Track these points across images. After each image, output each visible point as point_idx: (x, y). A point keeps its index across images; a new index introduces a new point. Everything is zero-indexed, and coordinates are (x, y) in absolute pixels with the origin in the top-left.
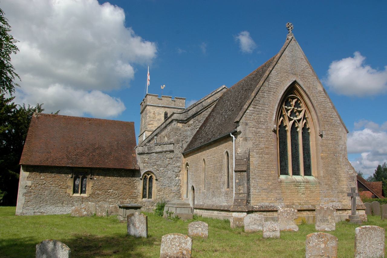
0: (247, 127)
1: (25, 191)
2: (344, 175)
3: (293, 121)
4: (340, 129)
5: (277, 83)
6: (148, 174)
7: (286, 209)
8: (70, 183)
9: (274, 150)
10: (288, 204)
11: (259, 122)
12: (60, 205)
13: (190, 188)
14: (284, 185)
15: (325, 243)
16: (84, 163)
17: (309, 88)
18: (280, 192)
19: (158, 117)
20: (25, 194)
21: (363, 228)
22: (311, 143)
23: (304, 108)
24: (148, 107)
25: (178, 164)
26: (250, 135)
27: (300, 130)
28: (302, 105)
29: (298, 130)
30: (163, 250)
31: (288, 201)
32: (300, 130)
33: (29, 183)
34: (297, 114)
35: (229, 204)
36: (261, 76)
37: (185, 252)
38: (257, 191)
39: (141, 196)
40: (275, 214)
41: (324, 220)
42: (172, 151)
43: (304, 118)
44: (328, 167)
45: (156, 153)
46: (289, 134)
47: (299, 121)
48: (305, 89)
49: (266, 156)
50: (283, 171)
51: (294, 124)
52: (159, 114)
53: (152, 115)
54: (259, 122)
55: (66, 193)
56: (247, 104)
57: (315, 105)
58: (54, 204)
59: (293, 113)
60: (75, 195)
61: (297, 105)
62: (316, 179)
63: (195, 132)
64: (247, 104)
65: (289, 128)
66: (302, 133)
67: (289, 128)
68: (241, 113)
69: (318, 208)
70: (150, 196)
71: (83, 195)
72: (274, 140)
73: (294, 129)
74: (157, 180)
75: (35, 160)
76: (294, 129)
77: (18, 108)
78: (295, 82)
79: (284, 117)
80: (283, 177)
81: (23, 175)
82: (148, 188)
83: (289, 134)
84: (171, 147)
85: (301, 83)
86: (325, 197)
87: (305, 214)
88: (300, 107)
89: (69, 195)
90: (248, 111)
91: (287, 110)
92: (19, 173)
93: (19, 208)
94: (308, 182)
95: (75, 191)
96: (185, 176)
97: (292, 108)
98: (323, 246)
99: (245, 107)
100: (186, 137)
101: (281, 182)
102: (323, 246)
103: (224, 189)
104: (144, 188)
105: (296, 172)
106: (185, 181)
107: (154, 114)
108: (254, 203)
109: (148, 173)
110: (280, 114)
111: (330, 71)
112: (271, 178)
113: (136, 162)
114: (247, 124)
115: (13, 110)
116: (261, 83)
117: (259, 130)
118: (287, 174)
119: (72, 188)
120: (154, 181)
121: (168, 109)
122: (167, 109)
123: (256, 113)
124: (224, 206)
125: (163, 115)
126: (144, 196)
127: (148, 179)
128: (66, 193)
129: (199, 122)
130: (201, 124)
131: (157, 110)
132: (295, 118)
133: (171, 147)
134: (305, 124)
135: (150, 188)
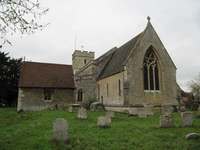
0: (129, 68)
1: (21, 99)
2: (174, 89)
3: (150, 65)
4: (173, 68)
5: (143, 47)
6: (80, 90)
7: (148, 106)
8: (43, 96)
9: (142, 78)
10: (149, 103)
11: (134, 65)
12: (38, 106)
13: (100, 96)
14: (146, 94)
15: (168, 120)
16: (49, 85)
17: (158, 48)
18: (145, 97)
19: (81, 62)
20: (21, 101)
21: (185, 113)
22: (159, 75)
23: (155, 58)
24: (76, 57)
25: (94, 85)
26: (130, 72)
27: (153, 69)
28: (155, 56)
29: (153, 69)
30: (99, 123)
31: (148, 102)
32: (153, 69)
33: (23, 96)
34: (152, 61)
35: (121, 104)
36: (135, 43)
37: (108, 124)
38: (134, 97)
39: (77, 101)
40: (143, 109)
41: (166, 111)
42: (91, 79)
43: (156, 63)
44: (167, 86)
45: (84, 80)
46: (148, 71)
47: (153, 64)
48: (156, 49)
49: (138, 81)
50: (146, 88)
51: (151, 66)
52: (82, 60)
53: (78, 61)
54: (134, 65)
55: (41, 100)
56: (129, 56)
57: (161, 56)
58: (36, 105)
59: (151, 61)
60: (46, 101)
61: (152, 57)
62: (161, 92)
63: (102, 70)
64: (129, 56)
65: (148, 68)
66: (155, 70)
67: (148, 68)
68: (126, 61)
69: (162, 105)
70: (81, 101)
71: (49, 101)
72: (142, 72)
73: (151, 67)
74: (84, 93)
75: (26, 84)
76: (151, 67)
77: (11, 59)
78: (151, 45)
79: (146, 63)
80: (146, 91)
81: (20, 91)
82: (80, 96)
83: (148, 71)
84: (91, 77)
85: (154, 46)
86: (166, 100)
87: (156, 108)
88: (154, 58)
89: (43, 101)
90: (129, 60)
91: (148, 59)
92: (18, 90)
93: (20, 105)
94: (157, 93)
95: (46, 99)
96: (98, 91)
97: (150, 58)
98: (167, 121)
99: (128, 58)
100: (98, 72)
101: (145, 93)
102: (167, 121)
103: (118, 97)
104: (79, 97)
105: (152, 89)
106: (98, 93)
107: (79, 60)
108: (131, 103)
109: (80, 90)
110: (145, 61)
111: (187, 93)
112: (140, 91)
113: (74, 85)
114: (129, 66)
115: (9, 59)
116: (135, 47)
117: (134, 69)
118: (148, 89)
119: (44, 98)
120: (83, 93)
121: (87, 58)
122: (86, 58)
123: (133, 61)
124: (118, 105)
125: (84, 61)
126: (79, 101)
127: (80, 93)
128: (41, 100)
129: (104, 64)
130: (105, 66)
131: (81, 58)
132: (151, 63)
133: (91, 77)
134: (156, 66)
135: (81, 97)
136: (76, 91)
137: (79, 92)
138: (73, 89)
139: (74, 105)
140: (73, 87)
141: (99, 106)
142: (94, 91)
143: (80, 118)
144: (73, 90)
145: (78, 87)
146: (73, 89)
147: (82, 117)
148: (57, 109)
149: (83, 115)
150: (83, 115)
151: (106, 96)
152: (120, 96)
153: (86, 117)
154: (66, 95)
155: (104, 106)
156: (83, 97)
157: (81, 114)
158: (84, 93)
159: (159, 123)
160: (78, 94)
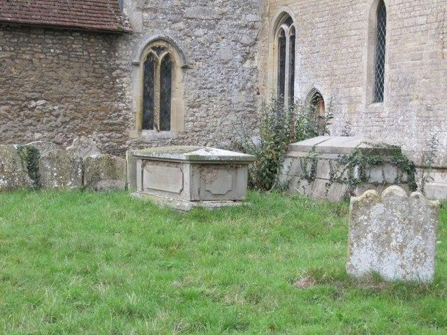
6: (159, 50)
25: (251, 18)
39: (138, 124)
70: (165, 126)
74: (185, 68)
96: (273, 58)
104: (147, 98)
109: (157, 46)
120: (178, 74)
126: (147, 124)
127: (159, 70)
135: (166, 96)
136: (132, 54)
137: (149, 65)
138: (113, 37)
139: (202, 152)
140: (115, 27)
141: (379, 164)
142: (247, 57)
143: (376, 278)
144: (112, 49)
145: (145, 24)
146: (113, 37)
147: (391, 270)
148: (38, 186)
149: (402, 248)
150: (402, 248)
151: (363, 91)
152: (379, 95)
153: (426, 273)
154: (59, 80)
155: (413, 167)
156: (179, 101)
157: (382, 241)
158: (185, 68)
159: (222, 207)
160: (145, 74)
